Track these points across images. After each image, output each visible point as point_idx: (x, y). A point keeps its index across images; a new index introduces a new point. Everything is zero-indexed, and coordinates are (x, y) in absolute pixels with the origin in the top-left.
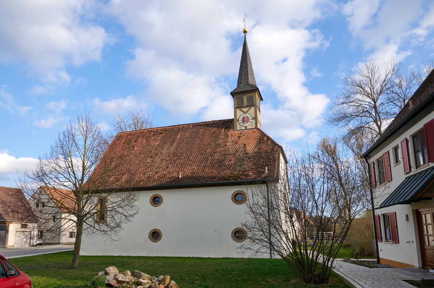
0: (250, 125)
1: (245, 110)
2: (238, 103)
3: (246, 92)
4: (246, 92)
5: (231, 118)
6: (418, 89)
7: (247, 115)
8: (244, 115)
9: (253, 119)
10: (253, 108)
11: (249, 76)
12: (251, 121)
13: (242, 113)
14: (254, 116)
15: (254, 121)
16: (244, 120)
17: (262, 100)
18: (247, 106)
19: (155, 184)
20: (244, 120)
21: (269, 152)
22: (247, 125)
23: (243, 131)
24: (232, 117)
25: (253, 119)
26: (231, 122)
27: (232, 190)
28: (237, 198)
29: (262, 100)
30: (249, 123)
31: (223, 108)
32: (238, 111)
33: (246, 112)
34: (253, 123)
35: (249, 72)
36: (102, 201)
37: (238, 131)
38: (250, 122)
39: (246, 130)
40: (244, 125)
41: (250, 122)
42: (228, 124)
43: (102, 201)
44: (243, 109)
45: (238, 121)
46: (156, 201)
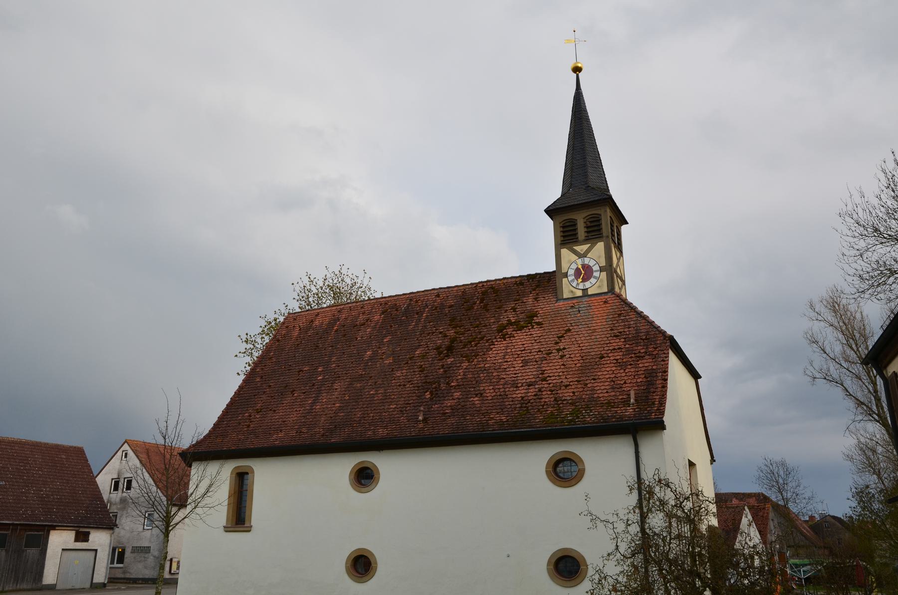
0: (597, 285)
1: (582, 248)
2: (563, 232)
3: (586, 209)
4: (586, 209)
5: (551, 270)
6: (241, 388)
7: (587, 261)
8: (580, 262)
9: (602, 269)
10: (600, 246)
11: (590, 170)
12: (596, 274)
13: (574, 257)
14: (603, 264)
15: (604, 274)
16: (585, 273)
17: (626, 223)
18: (587, 240)
19: (382, 432)
20: (585, 273)
21: (649, 347)
22: (588, 284)
23: (580, 300)
24: (552, 268)
25: (602, 269)
26: (549, 280)
27: (545, 452)
28: (560, 469)
29: (626, 223)
30: (593, 280)
31: (533, 249)
32: (565, 252)
33: (584, 255)
34: (602, 281)
35: (589, 159)
36: (242, 481)
37: (566, 302)
38: (595, 277)
39: (586, 299)
40: (581, 286)
41: (595, 277)
42: (544, 283)
43: (242, 481)
44: (578, 248)
45: (566, 275)
46: (364, 477)
